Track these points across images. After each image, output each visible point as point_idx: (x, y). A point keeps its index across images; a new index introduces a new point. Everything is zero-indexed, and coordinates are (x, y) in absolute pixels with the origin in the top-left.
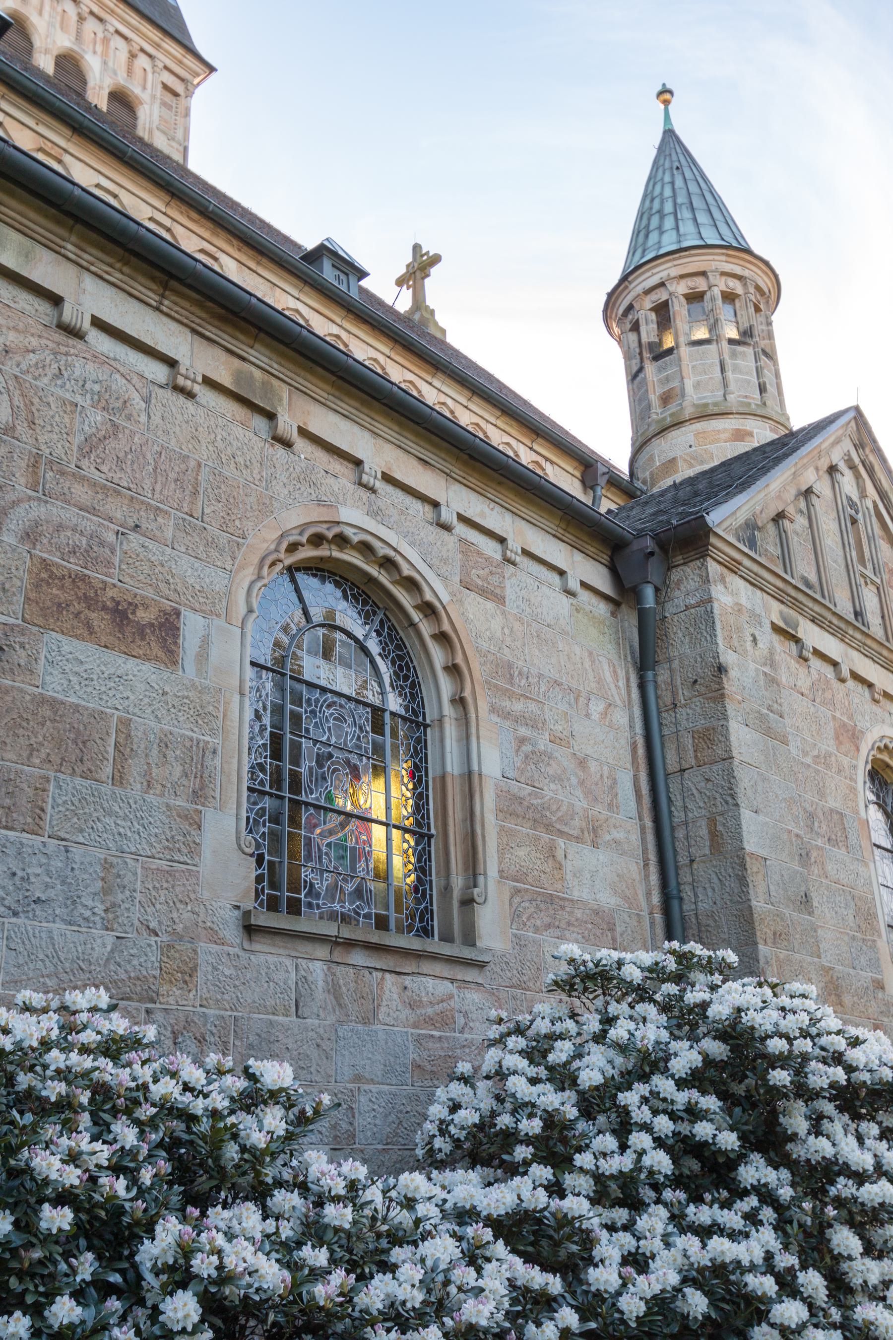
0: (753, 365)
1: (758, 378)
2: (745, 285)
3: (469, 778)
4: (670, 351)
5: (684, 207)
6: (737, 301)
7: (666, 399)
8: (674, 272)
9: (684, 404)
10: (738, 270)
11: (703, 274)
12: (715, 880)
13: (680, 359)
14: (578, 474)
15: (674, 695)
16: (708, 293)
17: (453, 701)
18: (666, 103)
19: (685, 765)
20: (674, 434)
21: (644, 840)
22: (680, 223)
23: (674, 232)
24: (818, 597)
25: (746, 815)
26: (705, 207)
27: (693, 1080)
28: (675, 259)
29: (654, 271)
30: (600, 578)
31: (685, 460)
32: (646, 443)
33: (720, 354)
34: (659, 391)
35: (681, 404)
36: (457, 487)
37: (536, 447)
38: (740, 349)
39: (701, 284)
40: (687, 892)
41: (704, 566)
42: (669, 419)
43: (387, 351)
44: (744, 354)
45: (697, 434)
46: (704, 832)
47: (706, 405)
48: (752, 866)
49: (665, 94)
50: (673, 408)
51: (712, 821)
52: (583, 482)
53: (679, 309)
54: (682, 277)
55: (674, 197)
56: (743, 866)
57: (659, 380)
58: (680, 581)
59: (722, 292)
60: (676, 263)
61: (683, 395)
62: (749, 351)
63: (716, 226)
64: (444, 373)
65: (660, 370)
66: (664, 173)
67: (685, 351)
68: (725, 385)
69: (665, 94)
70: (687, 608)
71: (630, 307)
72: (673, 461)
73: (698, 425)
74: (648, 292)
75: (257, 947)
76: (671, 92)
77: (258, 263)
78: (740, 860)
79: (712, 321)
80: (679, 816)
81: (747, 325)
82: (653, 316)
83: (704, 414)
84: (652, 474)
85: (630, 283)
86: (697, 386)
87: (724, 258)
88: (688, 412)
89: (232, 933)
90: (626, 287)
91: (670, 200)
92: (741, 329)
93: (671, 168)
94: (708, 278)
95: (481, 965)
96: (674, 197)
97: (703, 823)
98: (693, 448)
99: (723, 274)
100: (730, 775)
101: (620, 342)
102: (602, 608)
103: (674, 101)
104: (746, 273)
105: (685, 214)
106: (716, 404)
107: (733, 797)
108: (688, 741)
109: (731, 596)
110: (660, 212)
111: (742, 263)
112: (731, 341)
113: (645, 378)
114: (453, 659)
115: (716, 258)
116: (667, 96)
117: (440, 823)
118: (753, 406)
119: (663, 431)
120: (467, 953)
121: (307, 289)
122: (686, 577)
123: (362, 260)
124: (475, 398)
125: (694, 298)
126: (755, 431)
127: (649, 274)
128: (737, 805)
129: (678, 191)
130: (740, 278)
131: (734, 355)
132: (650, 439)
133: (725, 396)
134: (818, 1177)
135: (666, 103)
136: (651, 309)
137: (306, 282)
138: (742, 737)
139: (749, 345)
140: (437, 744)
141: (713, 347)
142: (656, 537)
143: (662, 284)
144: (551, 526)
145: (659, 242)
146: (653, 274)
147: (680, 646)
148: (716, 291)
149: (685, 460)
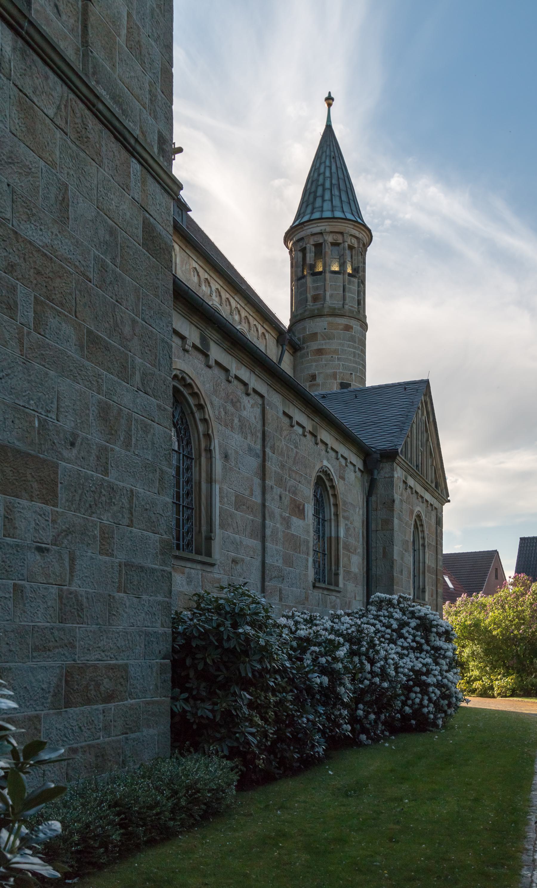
0: (357, 289)
1: (358, 297)
2: (359, 243)
3: (338, 538)
4: (320, 273)
5: (335, 186)
6: (354, 250)
7: (315, 298)
8: (328, 229)
9: (325, 305)
10: (357, 234)
11: (342, 233)
12: (383, 565)
13: (325, 280)
14: (276, 337)
15: (377, 506)
16: (342, 244)
17: (334, 514)
18: (329, 105)
19: (378, 529)
20: (318, 319)
21: (363, 551)
22: (333, 197)
23: (330, 203)
24: (420, 474)
25: (395, 546)
26: (345, 190)
27: (416, 628)
28: (329, 222)
29: (319, 225)
30: (359, 464)
31: (321, 335)
32: (302, 320)
33: (344, 282)
34: (312, 293)
35: (323, 304)
36: (341, 445)
37: (265, 326)
38: (353, 279)
39: (340, 239)
40: (374, 568)
41: (392, 465)
42: (316, 311)
43: (243, 305)
44: (354, 282)
45: (329, 323)
46: (381, 551)
47: (335, 309)
48: (395, 563)
49: (329, 100)
50: (318, 305)
51: (384, 548)
52: (278, 341)
53: (328, 249)
54: (331, 232)
55: (331, 178)
56: (393, 564)
57: (313, 287)
58: (382, 468)
59: (348, 245)
60: (330, 224)
61: (325, 299)
62: (356, 280)
63: (350, 203)
64: (241, 295)
65: (314, 281)
66: (326, 158)
67: (328, 275)
68: (344, 299)
69: (329, 100)
70: (385, 477)
71: (302, 239)
72: (316, 334)
73: (330, 318)
74: (313, 235)
75: (314, 591)
76: (333, 99)
77: (186, 246)
78: (392, 561)
79: (342, 261)
80: (374, 545)
81: (356, 265)
82: (313, 249)
83: (334, 314)
84: (304, 337)
85: (305, 226)
86: (331, 296)
87: (352, 226)
88: (326, 311)
89: (311, 588)
90: (302, 228)
91: (329, 179)
92: (354, 268)
93: (330, 156)
94: (343, 236)
95: (339, 592)
96: (331, 178)
97: (381, 548)
98: (326, 330)
99: (351, 235)
100: (392, 535)
101: (291, 252)
102: (359, 474)
103: (334, 103)
104: (360, 236)
105: (336, 192)
106: (339, 309)
107: (392, 542)
108: (380, 521)
109: (399, 474)
110: (323, 185)
111: (359, 230)
112: (349, 275)
113: (306, 281)
114: (204, 416)
115: (349, 226)
116: (331, 101)
117: (329, 550)
118: (355, 313)
119: (313, 317)
120: (337, 589)
121: (201, 258)
122: (386, 466)
123: (190, 205)
124: (248, 305)
125: (335, 244)
126: (354, 326)
127: (316, 225)
128: (393, 545)
129: (333, 174)
130: (357, 238)
131: (350, 282)
132: (305, 319)
133: (343, 304)
134: (437, 649)
135: (329, 105)
136: (313, 245)
137: (201, 255)
138: (396, 521)
139: (356, 277)
140: (329, 528)
141: (341, 276)
142: (381, 454)
143: (321, 233)
144: (354, 450)
145: (322, 207)
146: (317, 226)
147: (380, 490)
148: (346, 244)
149: (321, 335)
